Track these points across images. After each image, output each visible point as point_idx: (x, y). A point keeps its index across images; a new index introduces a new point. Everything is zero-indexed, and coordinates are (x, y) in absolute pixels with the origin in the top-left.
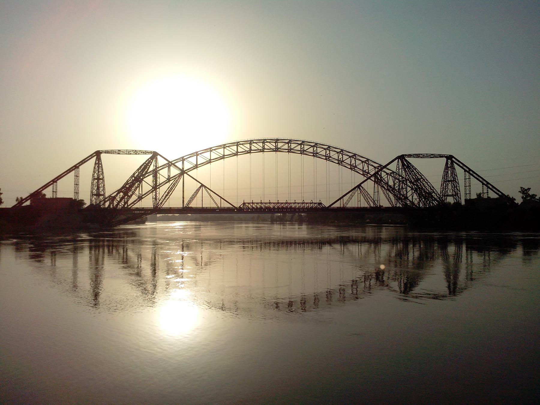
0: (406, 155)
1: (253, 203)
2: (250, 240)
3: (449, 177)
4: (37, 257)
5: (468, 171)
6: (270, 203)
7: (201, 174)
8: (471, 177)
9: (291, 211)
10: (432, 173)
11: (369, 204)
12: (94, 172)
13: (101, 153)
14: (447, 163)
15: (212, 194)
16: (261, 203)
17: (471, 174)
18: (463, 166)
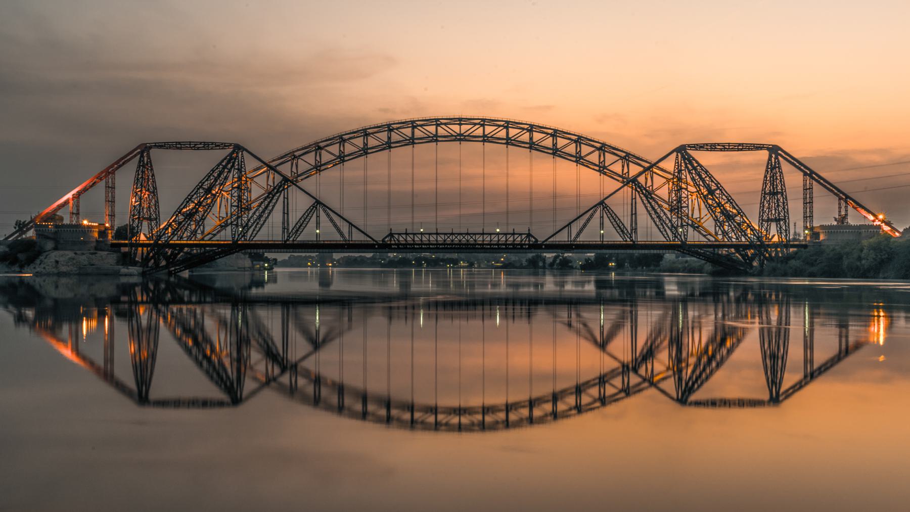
1: (437, 234)
2: (463, 299)
6: (437, 234)
7: (325, 184)
8: (814, 182)
14: (770, 159)
15: (582, 221)
16: (406, 234)
17: (813, 178)
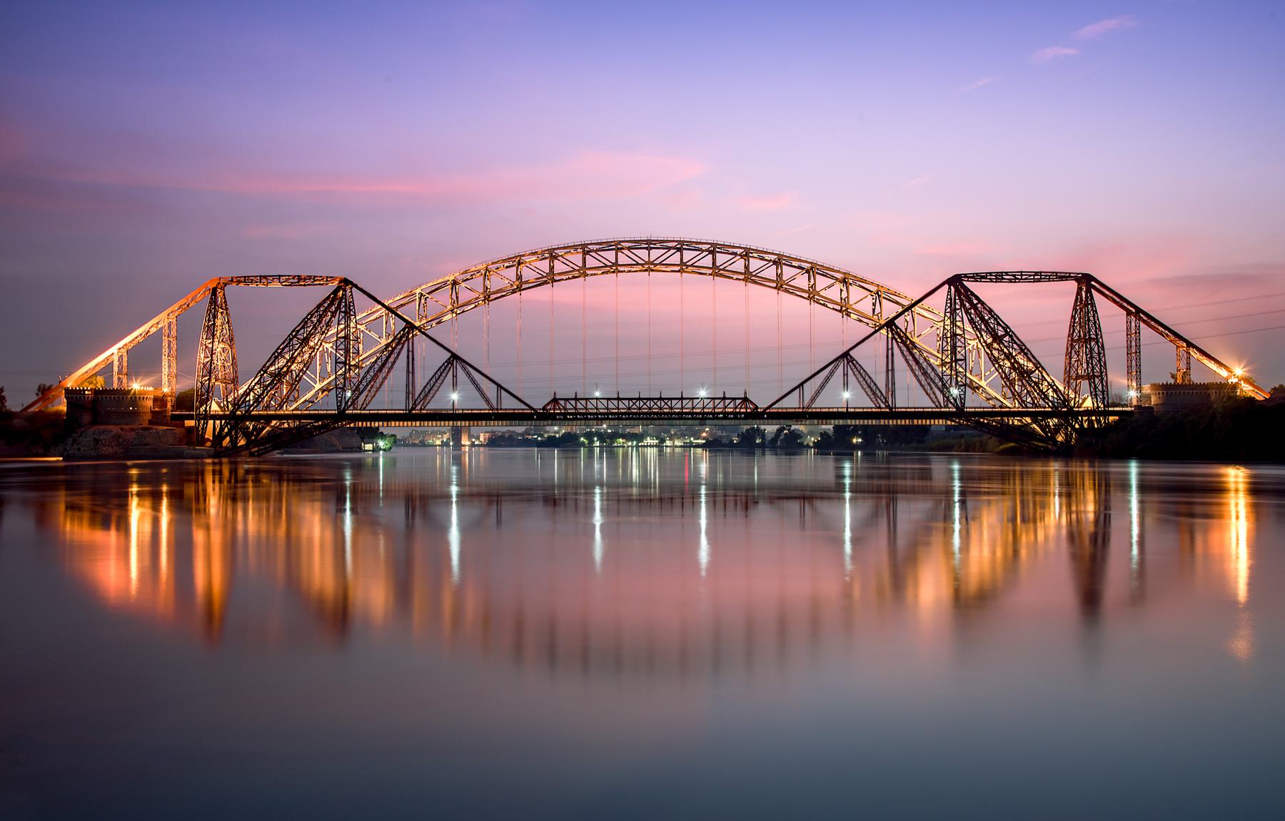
0: (965, 275)
3: (1084, 333)
4: (1275, 389)
5: (1136, 312)
6: (618, 399)
10: (1039, 316)
14: (1079, 293)
17: (1141, 319)
18: (1119, 300)
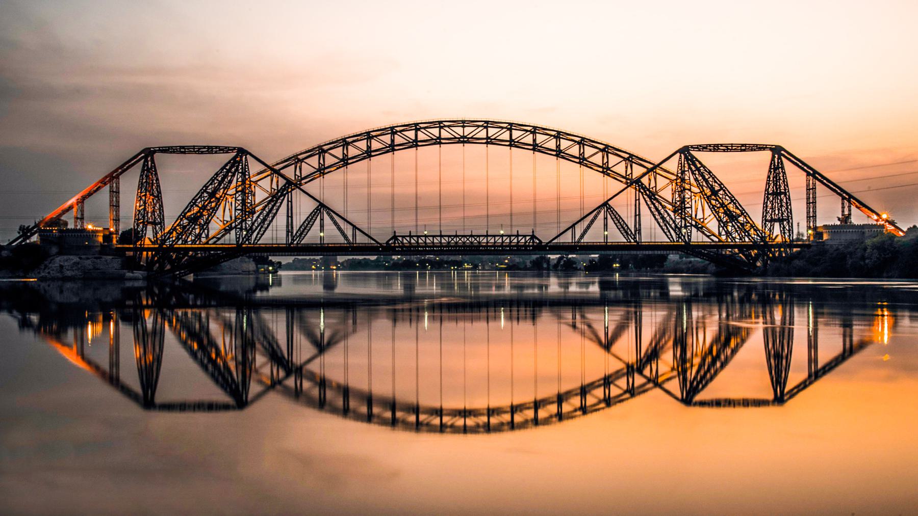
0: (692, 147)
1: (441, 236)
3: (776, 190)
5: (813, 174)
8: (818, 183)
9: (402, 250)
10: (745, 178)
11: (669, 236)
12: (212, 180)
13: (155, 152)
